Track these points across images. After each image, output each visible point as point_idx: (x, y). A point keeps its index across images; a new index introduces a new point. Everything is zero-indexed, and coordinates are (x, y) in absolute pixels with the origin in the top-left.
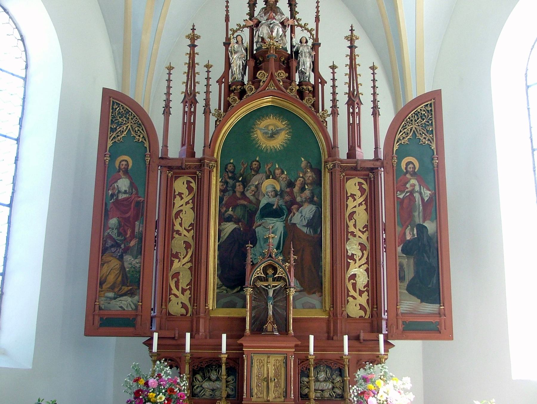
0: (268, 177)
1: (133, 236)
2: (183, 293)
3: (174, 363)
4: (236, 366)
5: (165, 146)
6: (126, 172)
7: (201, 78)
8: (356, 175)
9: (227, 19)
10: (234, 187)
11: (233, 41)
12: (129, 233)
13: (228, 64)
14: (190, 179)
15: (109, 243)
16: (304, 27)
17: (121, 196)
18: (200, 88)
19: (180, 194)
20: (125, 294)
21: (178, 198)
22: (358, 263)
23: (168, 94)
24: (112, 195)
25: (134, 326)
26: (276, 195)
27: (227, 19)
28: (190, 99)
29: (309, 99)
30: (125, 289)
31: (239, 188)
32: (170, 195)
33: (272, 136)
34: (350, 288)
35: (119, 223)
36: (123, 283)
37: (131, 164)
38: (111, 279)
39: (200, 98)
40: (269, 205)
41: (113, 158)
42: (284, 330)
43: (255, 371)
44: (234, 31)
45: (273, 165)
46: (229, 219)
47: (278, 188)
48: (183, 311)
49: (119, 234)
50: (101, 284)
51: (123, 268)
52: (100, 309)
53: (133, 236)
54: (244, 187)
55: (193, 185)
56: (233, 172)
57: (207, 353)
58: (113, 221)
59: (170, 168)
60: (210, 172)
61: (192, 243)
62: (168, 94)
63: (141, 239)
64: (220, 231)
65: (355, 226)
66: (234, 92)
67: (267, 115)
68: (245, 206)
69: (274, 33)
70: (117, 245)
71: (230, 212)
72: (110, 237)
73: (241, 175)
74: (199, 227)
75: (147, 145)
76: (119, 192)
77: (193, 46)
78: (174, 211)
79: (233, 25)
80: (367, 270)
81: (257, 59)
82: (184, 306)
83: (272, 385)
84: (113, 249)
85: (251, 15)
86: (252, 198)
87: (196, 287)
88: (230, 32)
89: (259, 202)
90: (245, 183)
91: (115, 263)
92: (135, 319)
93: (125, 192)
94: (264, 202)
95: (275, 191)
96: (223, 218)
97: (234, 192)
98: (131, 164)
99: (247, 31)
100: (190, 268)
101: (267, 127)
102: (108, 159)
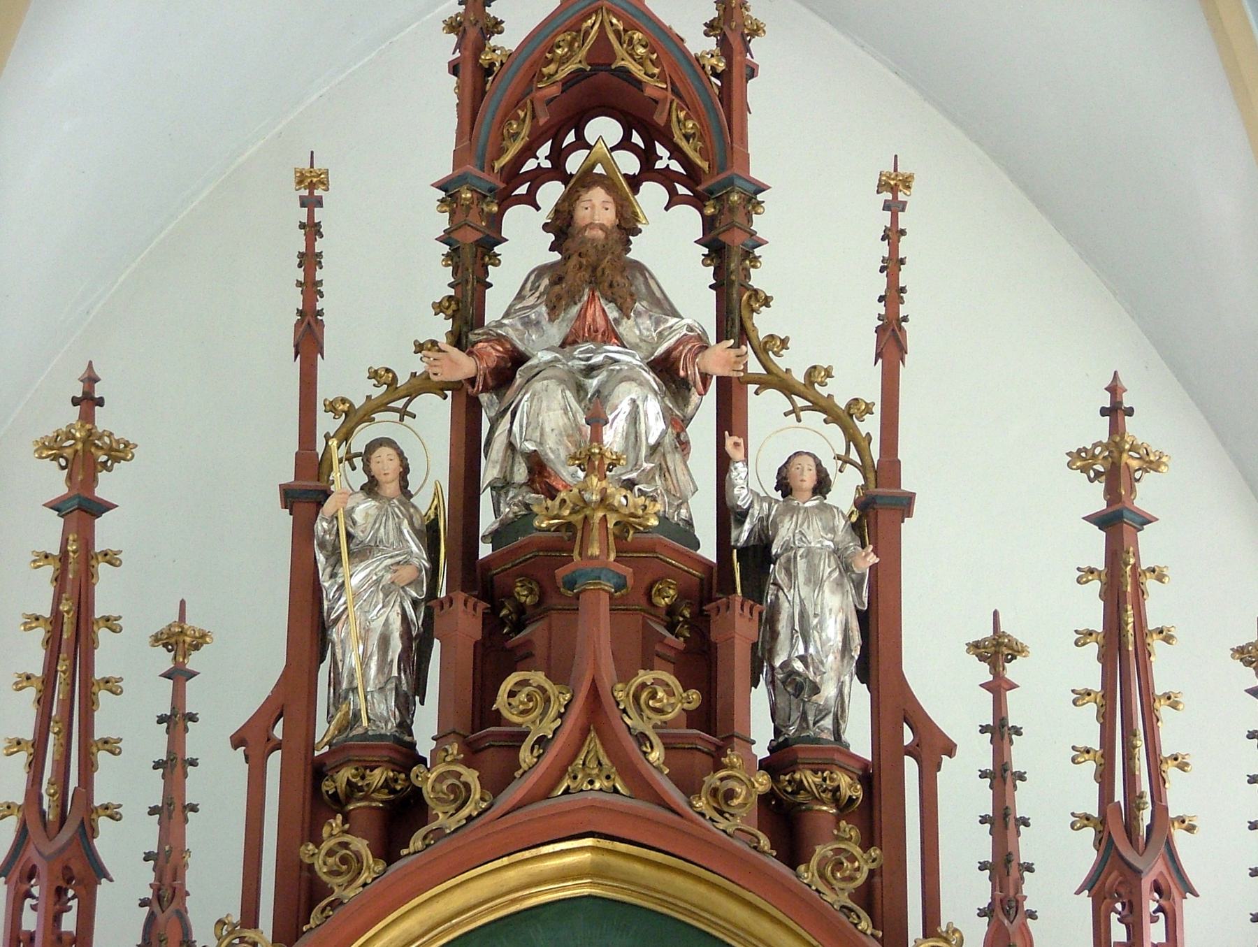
7: (129, 717)
9: (309, 338)
11: (346, 479)
13: (312, 627)
16: (806, 392)
18: (128, 783)
27: (309, 338)
29: (836, 848)
39: (124, 846)
44: (354, 417)
69: (618, 440)
77: (82, 509)
79: (343, 377)
81: (500, 592)
85: (464, 310)
88: (326, 423)
99: (435, 414)
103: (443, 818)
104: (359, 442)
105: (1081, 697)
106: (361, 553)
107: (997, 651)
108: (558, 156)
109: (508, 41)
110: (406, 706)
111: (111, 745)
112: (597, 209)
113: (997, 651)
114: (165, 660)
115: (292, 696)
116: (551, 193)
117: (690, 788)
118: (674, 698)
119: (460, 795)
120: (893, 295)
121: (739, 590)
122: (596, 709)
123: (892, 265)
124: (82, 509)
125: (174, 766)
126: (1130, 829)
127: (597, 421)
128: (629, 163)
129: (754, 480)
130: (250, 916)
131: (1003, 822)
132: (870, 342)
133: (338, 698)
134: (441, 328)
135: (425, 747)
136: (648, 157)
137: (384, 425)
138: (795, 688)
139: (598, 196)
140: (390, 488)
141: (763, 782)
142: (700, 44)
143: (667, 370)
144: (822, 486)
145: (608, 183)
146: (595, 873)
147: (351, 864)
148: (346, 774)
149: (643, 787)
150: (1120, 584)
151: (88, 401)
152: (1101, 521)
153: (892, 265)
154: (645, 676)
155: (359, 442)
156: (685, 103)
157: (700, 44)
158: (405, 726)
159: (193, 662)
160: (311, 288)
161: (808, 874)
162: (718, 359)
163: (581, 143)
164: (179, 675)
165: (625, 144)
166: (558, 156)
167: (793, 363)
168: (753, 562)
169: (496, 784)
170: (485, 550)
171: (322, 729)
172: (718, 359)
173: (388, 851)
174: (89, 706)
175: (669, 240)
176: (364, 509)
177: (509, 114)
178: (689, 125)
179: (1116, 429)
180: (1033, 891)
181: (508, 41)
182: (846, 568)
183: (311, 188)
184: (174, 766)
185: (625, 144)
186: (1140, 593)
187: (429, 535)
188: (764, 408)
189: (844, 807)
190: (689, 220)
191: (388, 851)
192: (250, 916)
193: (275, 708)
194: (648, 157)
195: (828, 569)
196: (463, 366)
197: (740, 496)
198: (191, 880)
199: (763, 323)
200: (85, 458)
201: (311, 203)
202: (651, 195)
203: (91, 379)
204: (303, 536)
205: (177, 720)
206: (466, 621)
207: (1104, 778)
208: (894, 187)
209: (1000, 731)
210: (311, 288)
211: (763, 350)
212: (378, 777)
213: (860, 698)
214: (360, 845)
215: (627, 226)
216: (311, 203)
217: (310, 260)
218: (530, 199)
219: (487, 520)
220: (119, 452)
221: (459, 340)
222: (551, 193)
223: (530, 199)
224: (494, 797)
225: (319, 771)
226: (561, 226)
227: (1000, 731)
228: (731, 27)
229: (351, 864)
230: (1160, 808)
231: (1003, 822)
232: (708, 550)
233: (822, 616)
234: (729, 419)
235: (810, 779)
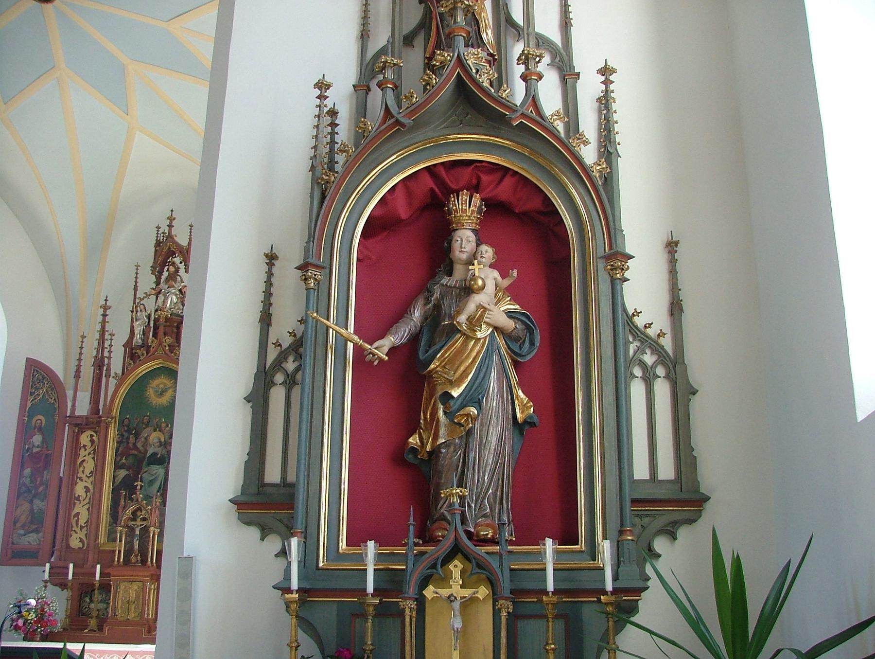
0: (155, 430)
1: (41, 484)
2: (81, 530)
3: (63, 586)
4: (105, 587)
5: (74, 406)
6: (40, 429)
8: (89, 429)
9: (136, 289)
10: (128, 438)
12: (39, 480)
14: (93, 433)
15: (24, 488)
17: (35, 450)
19: (84, 446)
20: (32, 532)
21: (83, 449)
22: (83, 503)
23: (80, 360)
24: (28, 449)
25: (37, 557)
26: (161, 445)
27: (136, 289)
28: (100, 364)
30: (34, 527)
31: (132, 439)
32: (76, 446)
33: (161, 394)
34: (74, 524)
35: (32, 472)
36: (32, 522)
37: (44, 422)
38: (23, 519)
40: (155, 454)
41: (30, 417)
42: (144, 562)
43: (121, 596)
44: (141, 300)
45: (160, 419)
46: (121, 467)
47: (163, 440)
48: (81, 545)
49: (31, 482)
50: (15, 523)
51: (32, 510)
52: (13, 543)
53: (41, 484)
54: (136, 438)
55: (95, 438)
56: (128, 426)
57: (86, 579)
58: (28, 471)
59: (77, 425)
60: (107, 428)
61: (91, 487)
62: (80, 360)
63: (47, 485)
64: (114, 477)
65: (83, 472)
66: (132, 354)
67: (159, 375)
68: (135, 455)
70: (29, 491)
71: (124, 461)
72: (24, 484)
73: (135, 429)
74: (98, 474)
75: (56, 406)
76: (34, 446)
77: (105, 315)
78: (80, 460)
79: (140, 294)
80: (88, 509)
82: (81, 540)
83: (132, 607)
84: (26, 495)
85: (158, 283)
86: (141, 448)
87: (93, 525)
88: (137, 301)
89: (146, 451)
90: (137, 436)
91: (26, 506)
92: (38, 552)
93: (38, 447)
94: (150, 451)
95: (160, 442)
96: (117, 466)
97: (128, 443)
98: (44, 422)
100: (88, 509)
101: (158, 385)
102: (26, 419)
121: (60, 645)
132: (274, 320)
149: (166, 354)
169: (147, 353)
198: (112, 367)
200: (106, 308)
210: (136, 282)
224: (12, 558)
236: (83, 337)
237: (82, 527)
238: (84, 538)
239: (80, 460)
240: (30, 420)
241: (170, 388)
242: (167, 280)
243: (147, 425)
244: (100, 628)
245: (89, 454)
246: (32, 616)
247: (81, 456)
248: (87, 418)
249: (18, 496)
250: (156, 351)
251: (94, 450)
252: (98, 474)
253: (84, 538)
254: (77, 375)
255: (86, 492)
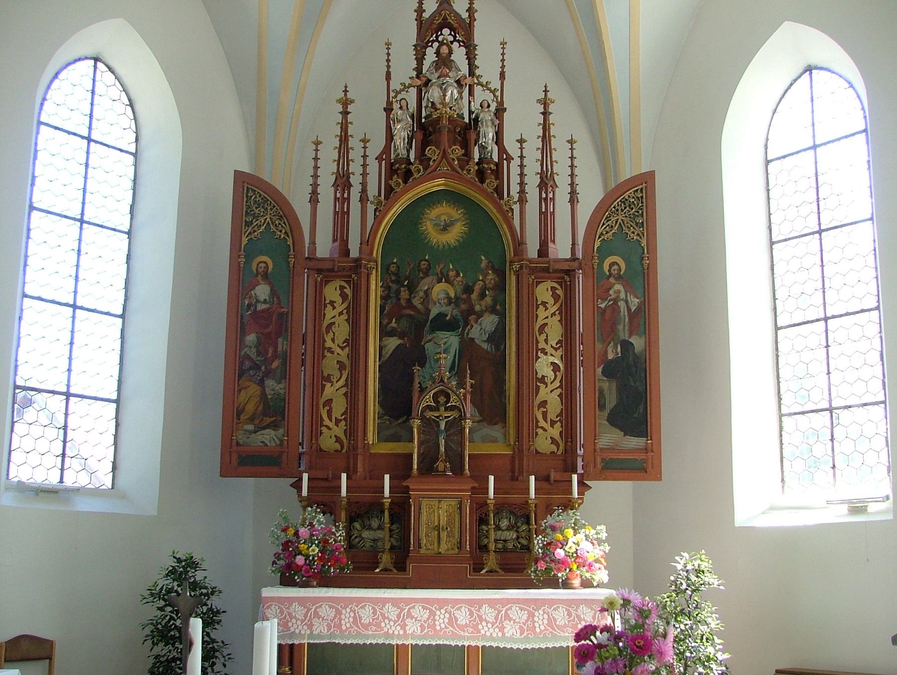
0: (439, 281)
6: (266, 276)
7: (356, 154)
9: (388, 76)
10: (398, 292)
11: (396, 106)
12: (271, 351)
13: (390, 136)
14: (344, 284)
15: (247, 364)
16: (486, 86)
17: (260, 307)
18: (355, 168)
20: (264, 428)
21: (329, 307)
24: (249, 306)
27: (388, 76)
28: (342, 181)
30: (268, 420)
31: (404, 294)
32: (319, 304)
34: (540, 417)
35: (258, 338)
36: (265, 414)
37: (271, 266)
38: (250, 408)
39: (356, 180)
40: (441, 315)
41: (249, 258)
43: (424, 518)
44: (397, 93)
46: (392, 333)
48: (338, 446)
51: (263, 394)
52: (238, 444)
53: (275, 356)
54: (411, 293)
55: (348, 291)
56: (396, 275)
58: (251, 338)
59: (319, 271)
60: (368, 276)
61: (347, 363)
65: (546, 341)
66: (398, 172)
68: (410, 316)
69: (448, 97)
71: (393, 324)
72: (248, 357)
74: (356, 343)
75: (290, 242)
76: (258, 301)
77: (345, 113)
78: (325, 324)
79: (395, 85)
81: (427, 130)
83: (444, 535)
85: (419, 70)
86: (420, 307)
88: (392, 94)
91: (254, 389)
93: (265, 301)
94: (434, 311)
96: (385, 332)
98: (271, 266)
99: (413, 91)
101: (438, 217)
103: (416, 176)
104: (399, 98)
105: (538, 149)
106: (399, 121)
107: (521, 141)
108: (437, 37)
109: (426, 15)
110: (408, 151)
111: (353, 161)
112: (445, 50)
113: (521, 141)
114: (362, 144)
115: (387, 149)
116: (436, 45)
117: (463, 169)
118: (459, 151)
119: (419, 171)
120: (503, 67)
122: (444, 155)
123: (503, 60)
124: (345, 113)
125: (364, 166)
126: (547, 176)
127: (445, 95)
128: (451, 38)
129: (475, 106)
130: (380, 195)
131: (522, 175)
133: (395, 151)
134: (414, 74)
135: (412, 161)
136: (455, 37)
137: (403, 95)
138: (483, 148)
139: (445, 47)
140: (405, 108)
141: (476, 167)
142: (465, 15)
143: (458, 82)
144: (489, 106)
145: (447, 44)
146: (444, 185)
147: (398, 184)
148: (397, 166)
149: (454, 169)
150: (546, 127)
151: (346, 91)
152: (543, 113)
153: (503, 60)
154: (454, 147)
155: (399, 98)
156: (462, 29)
157: (465, 15)
158: (408, 156)
159: (367, 145)
160: (388, 67)
161: (485, 185)
162: (469, 80)
163: (441, 34)
164: (365, 148)
165: (450, 34)
166: (437, 37)
167: (483, 80)
168: (476, 121)
169: (425, 169)
170: (423, 120)
171: (393, 156)
172: (469, 80)
173: (405, 182)
174: (348, 152)
175: (459, 55)
176: (400, 112)
177: (427, 31)
178: (465, 30)
179: (546, 95)
180: (527, 189)
181: (426, 15)
182: (493, 123)
183: (388, 44)
184: (364, 166)
185: (450, 34)
186: (549, 128)
187: (412, 117)
188: (478, 89)
189: (492, 171)
190: (463, 50)
191: (405, 182)
192: (380, 195)
193: (382, 153)
194: (455, 37)
195: (490, 123)
196: (419, 82)
197: (473, 109)
199: (477, 72)
200: (346, 103)
201: (388, 49)
202: (456, 44)
203: (346, 87)
204: (388, 117)
205: (365, 157)
206: (420, 135)
207: (542, 165)
208: (503, 44)
209: (522, 157)
210: (388, 67)
211: (478, 78)
212: (403, 166)
213: (496, 148)
214: (400, 181)
215: (451, 52)
216: (388, 49)
217: (388, 61)
218: (431, 46)
219: (424, 114)
220: (352, 102)
221: (418, 77)
222: (436, 45)
223: (431, 46)
225: (392, 165)
226: (438, 53)
227: (522, 157)
228: (471, 11)
229: (398, 184)
230: (552, 172)
231: (522, 175)
232: (467, 120)
233: (488, 133)
234: (471, 93)
235: (486, 166)
236: (317, 143)
237: (337, 422)
238: (343, 437)
239: (325, 324)
240: (249, 261)
241: (457, 220)
242: (437, 65)
243: (427, 274)
244: (400, 566)
245: (341, 314)
246: (315, 550)
247: (328, 316)
248: (331, 260)
249: (240, 377)
250: (438, 166)
251: (560, 309)
252: (356, 343)
253: (343, 437)
254: (314, 199)
255: (554, 371)
